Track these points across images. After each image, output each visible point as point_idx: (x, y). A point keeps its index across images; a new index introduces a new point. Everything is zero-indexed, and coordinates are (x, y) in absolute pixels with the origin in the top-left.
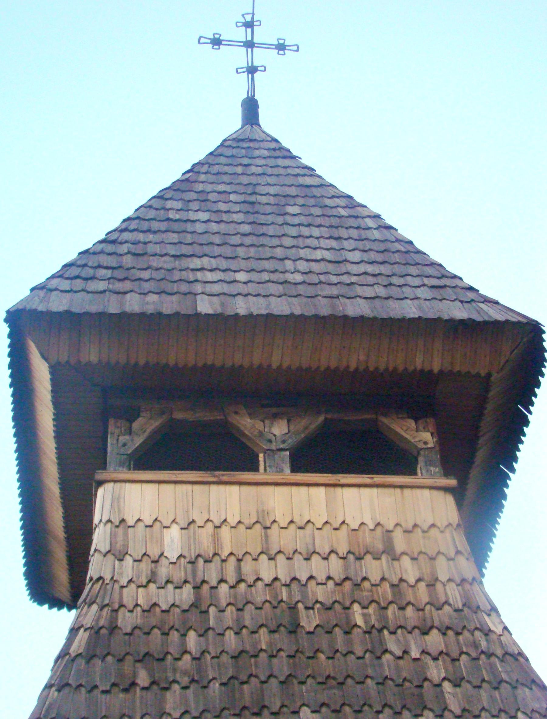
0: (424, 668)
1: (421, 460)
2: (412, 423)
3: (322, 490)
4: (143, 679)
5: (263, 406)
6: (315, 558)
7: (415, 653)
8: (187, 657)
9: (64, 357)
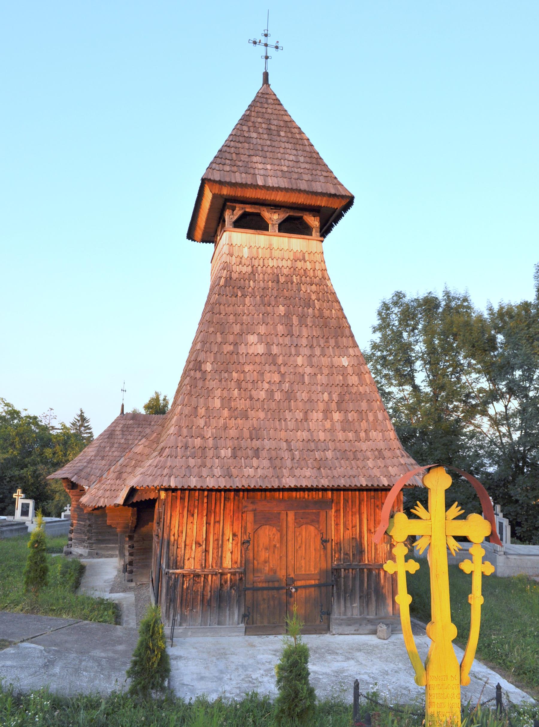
0: (310, 296)
1: (314, 230)
2: (313, 218)
3: (287, 239)
4: (240, 294)
5: (272, 209)
6: (284, 260)
7: (308, 291)
8: (250, 288)
9: (217, 192)
